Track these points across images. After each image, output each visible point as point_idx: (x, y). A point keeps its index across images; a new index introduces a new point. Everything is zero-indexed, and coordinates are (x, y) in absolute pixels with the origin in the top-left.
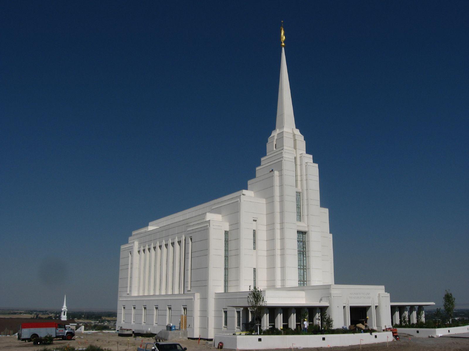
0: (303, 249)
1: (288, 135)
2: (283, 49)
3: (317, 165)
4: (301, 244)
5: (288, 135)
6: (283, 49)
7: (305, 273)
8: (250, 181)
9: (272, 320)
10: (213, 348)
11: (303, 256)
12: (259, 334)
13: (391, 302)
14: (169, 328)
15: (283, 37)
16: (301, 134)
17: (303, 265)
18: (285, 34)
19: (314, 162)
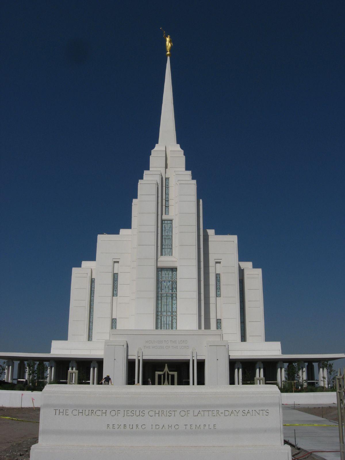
0: (172, 289)
1: (168, 151)
2: (169, 58)
3: (195, 182)
4: (168, 284)
5: (168, 151)
6: (169, 58)
7: (174, 321)
8: (252, 263)
9: (311, 375)
10: (61, 411)
11: (172, 299)
12: (308, 382)
13: (90, 382)
14: (239, 374)
15: (168, 45)
16: (182, 149)
17: (171, 311)
18: (170, 42)
19: (193, 179)
